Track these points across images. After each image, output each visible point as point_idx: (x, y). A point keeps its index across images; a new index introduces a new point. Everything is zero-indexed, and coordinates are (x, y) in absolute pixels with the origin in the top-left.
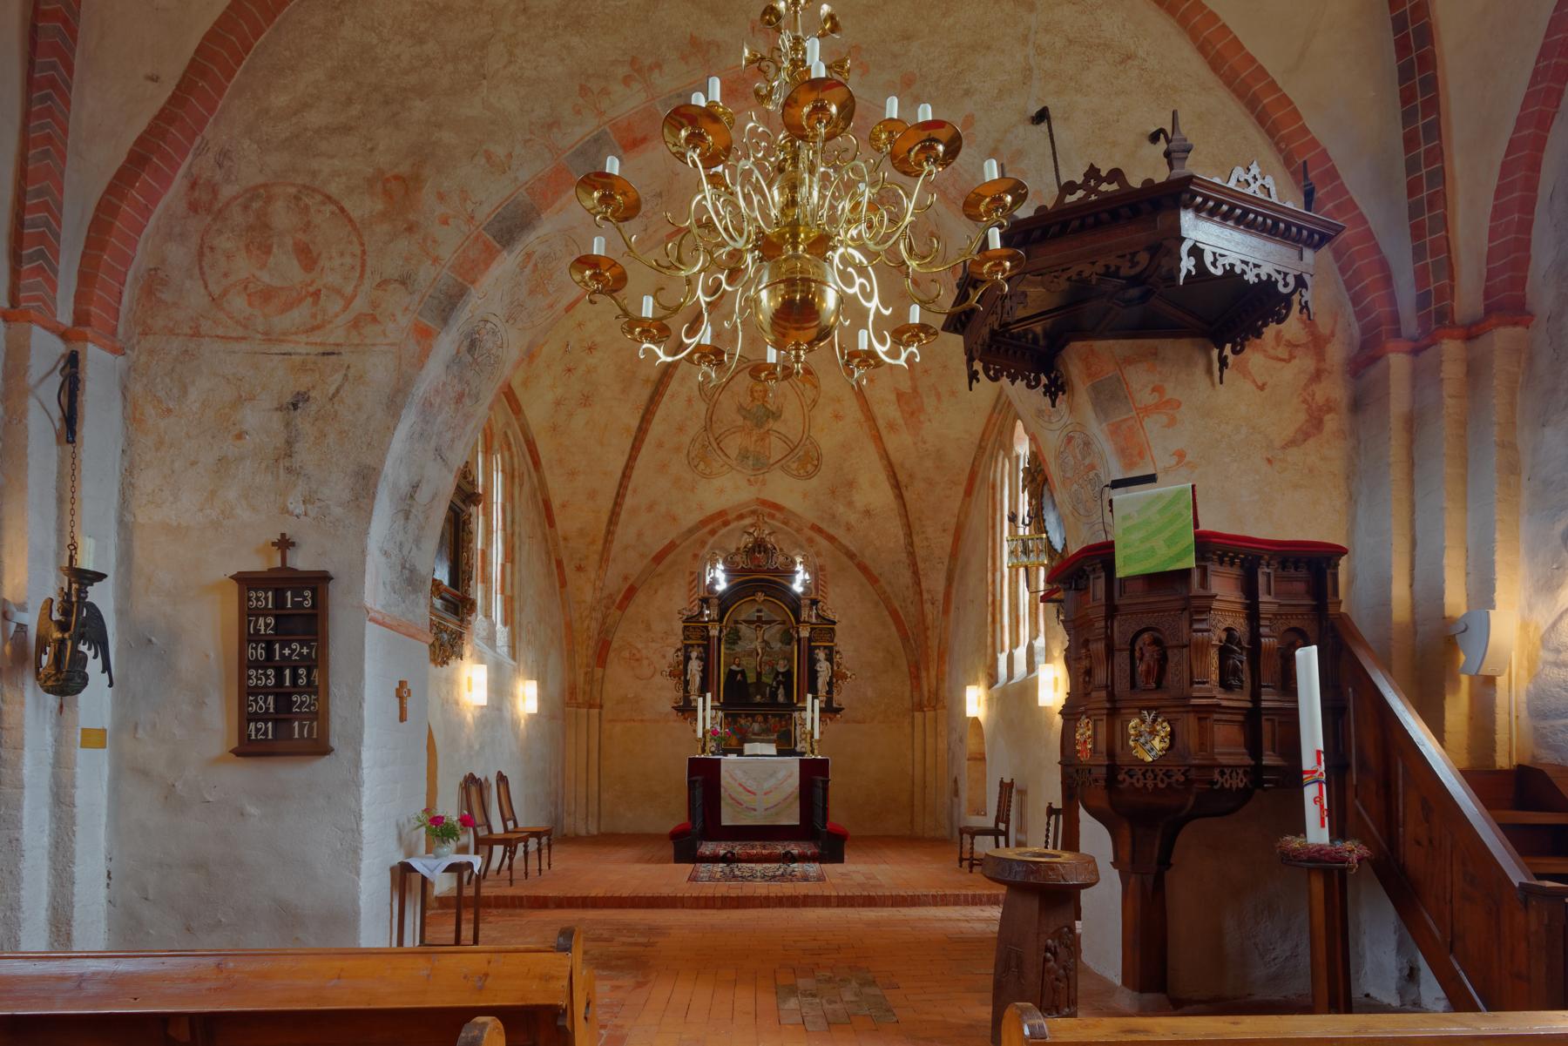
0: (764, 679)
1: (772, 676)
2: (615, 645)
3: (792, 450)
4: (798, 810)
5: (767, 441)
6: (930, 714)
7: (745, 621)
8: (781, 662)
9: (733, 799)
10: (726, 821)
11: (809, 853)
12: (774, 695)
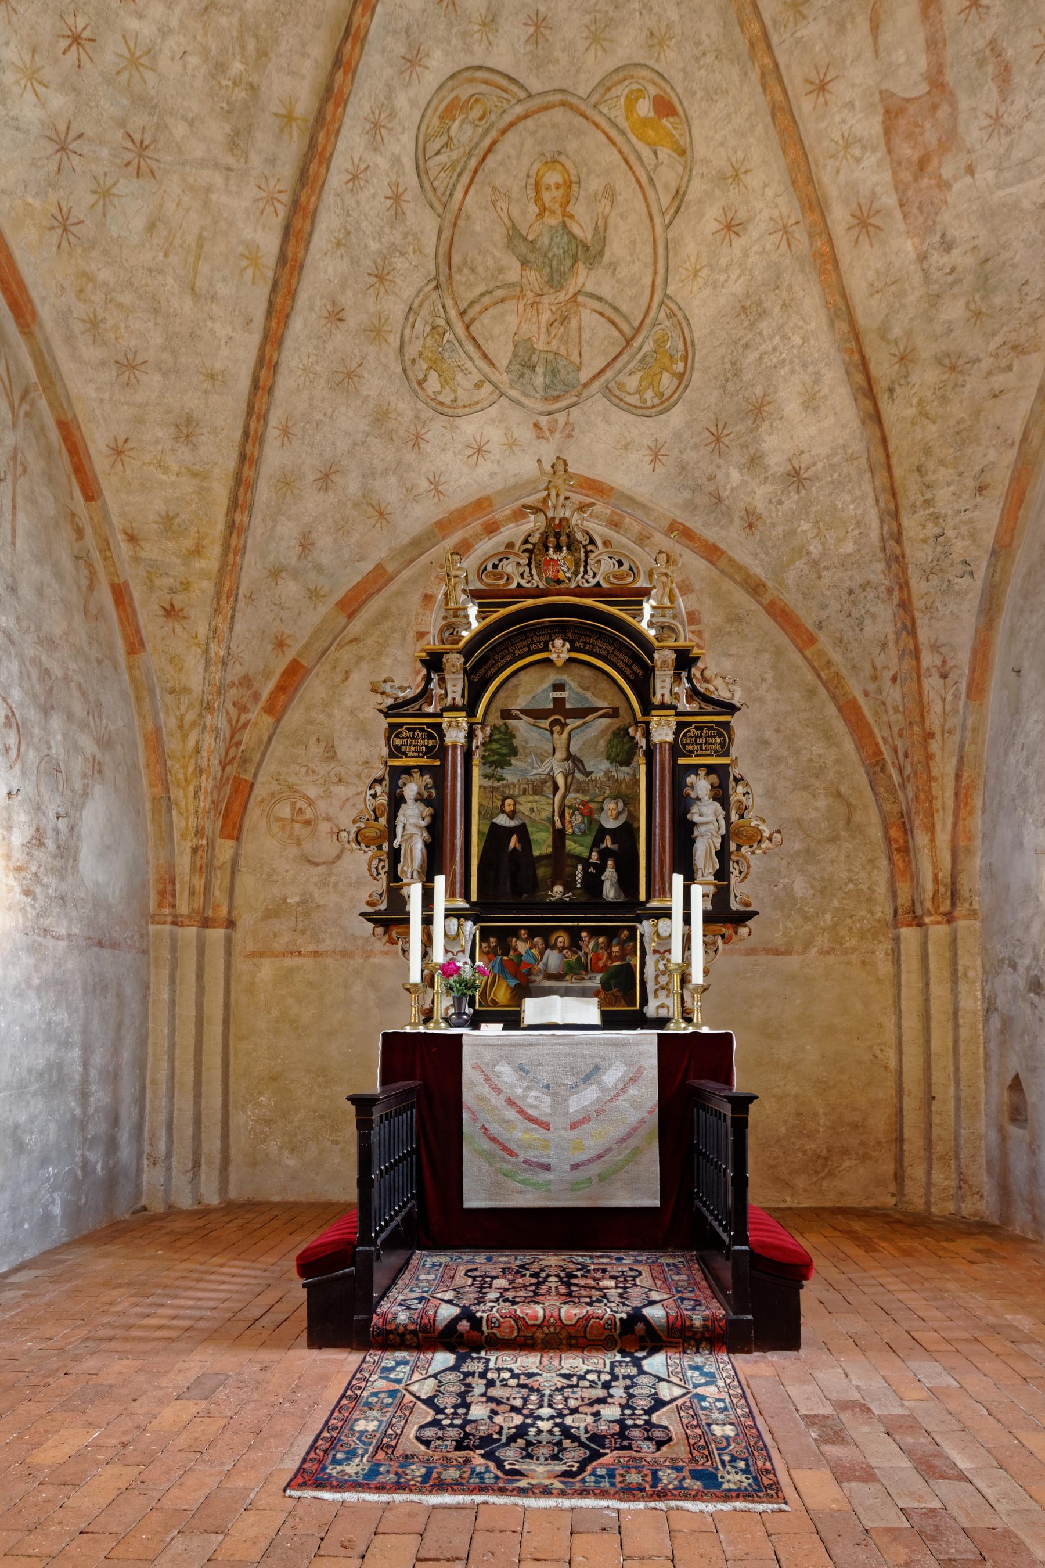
0: (571, 846)
1: (589, 840)
2: (260, 791)
3: (629, 342)
4: (656, 1168)
5: (574, 323)
6: (938, 931)
7: (526, 712)
8: (610, 806)
9: (493, 1139)
10: (474, 1198)
11: (698, 1321)
12: (593, 883)
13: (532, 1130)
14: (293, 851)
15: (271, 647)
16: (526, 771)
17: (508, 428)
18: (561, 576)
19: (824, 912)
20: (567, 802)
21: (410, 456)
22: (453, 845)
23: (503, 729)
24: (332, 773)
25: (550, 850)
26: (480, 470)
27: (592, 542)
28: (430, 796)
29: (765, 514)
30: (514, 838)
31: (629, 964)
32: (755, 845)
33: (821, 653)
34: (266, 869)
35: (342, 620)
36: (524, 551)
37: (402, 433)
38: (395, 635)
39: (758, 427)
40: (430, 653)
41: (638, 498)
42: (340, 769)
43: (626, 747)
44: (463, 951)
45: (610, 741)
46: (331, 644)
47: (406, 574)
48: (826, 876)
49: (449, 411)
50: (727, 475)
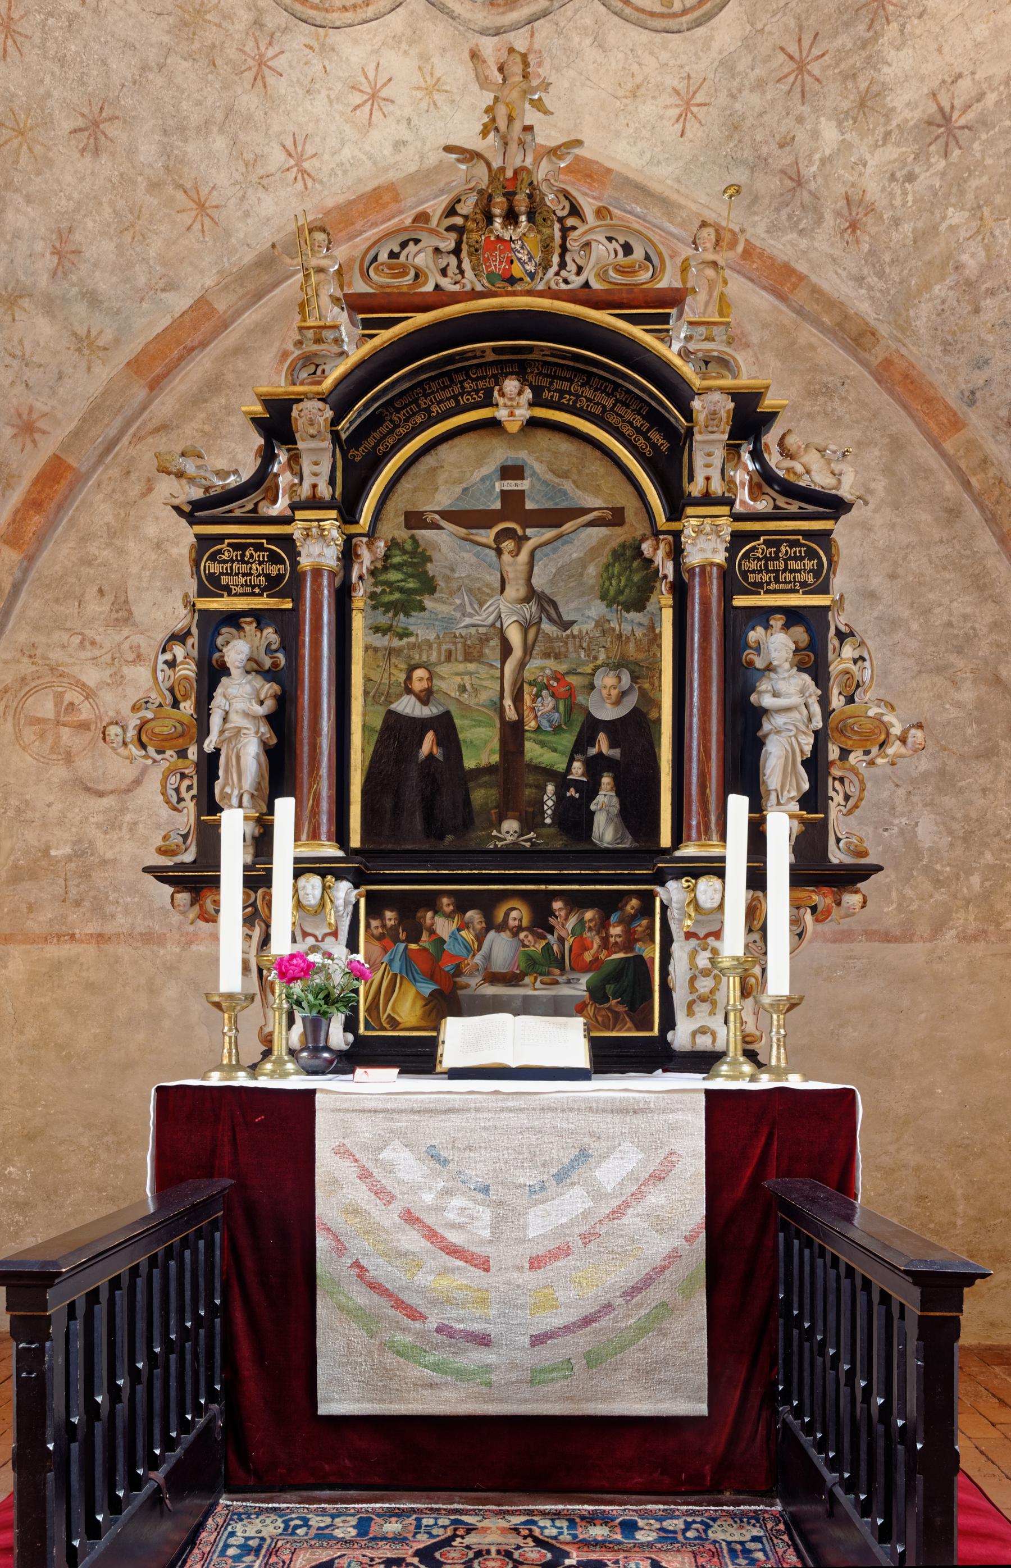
0: (533, 751)
1: (568, 740)
4: (701, 1343)
7: (451, 516)
8: (606, 681)
9: (376, 1287)
13: (453, 1270)
14: (60, 772)
15: (9, 432)
16: (450, 620)
17: (424, 58)
18: (517, 270)
19: (969, 873)
20: (527, 675)
21: (249, 101)
22: (314, 747)
23: (408, 546)
24: (126, 646)
25: (495, 758)
26: (375, 135)
27: (575, 211)
28: (275, 665)
29: (882, 202)
30: (430, 737)
31: (640, 957)
32: (875, 750)
33: (971, 446)
34: (14, 802)
35: (140, 393)
36: (449, 229)
37: (231, 53)
38: (233, 420)
39: (876, 38)
40: (268, 402)
41: (655, 187)
42: (137, 639)
43: (636, 578)
44: (335, 934)
45: (607, 566)
46: (122, 432)
47: (250, 318)
48: (974, 815)
49: (318, 16)
50: (815, 135)
